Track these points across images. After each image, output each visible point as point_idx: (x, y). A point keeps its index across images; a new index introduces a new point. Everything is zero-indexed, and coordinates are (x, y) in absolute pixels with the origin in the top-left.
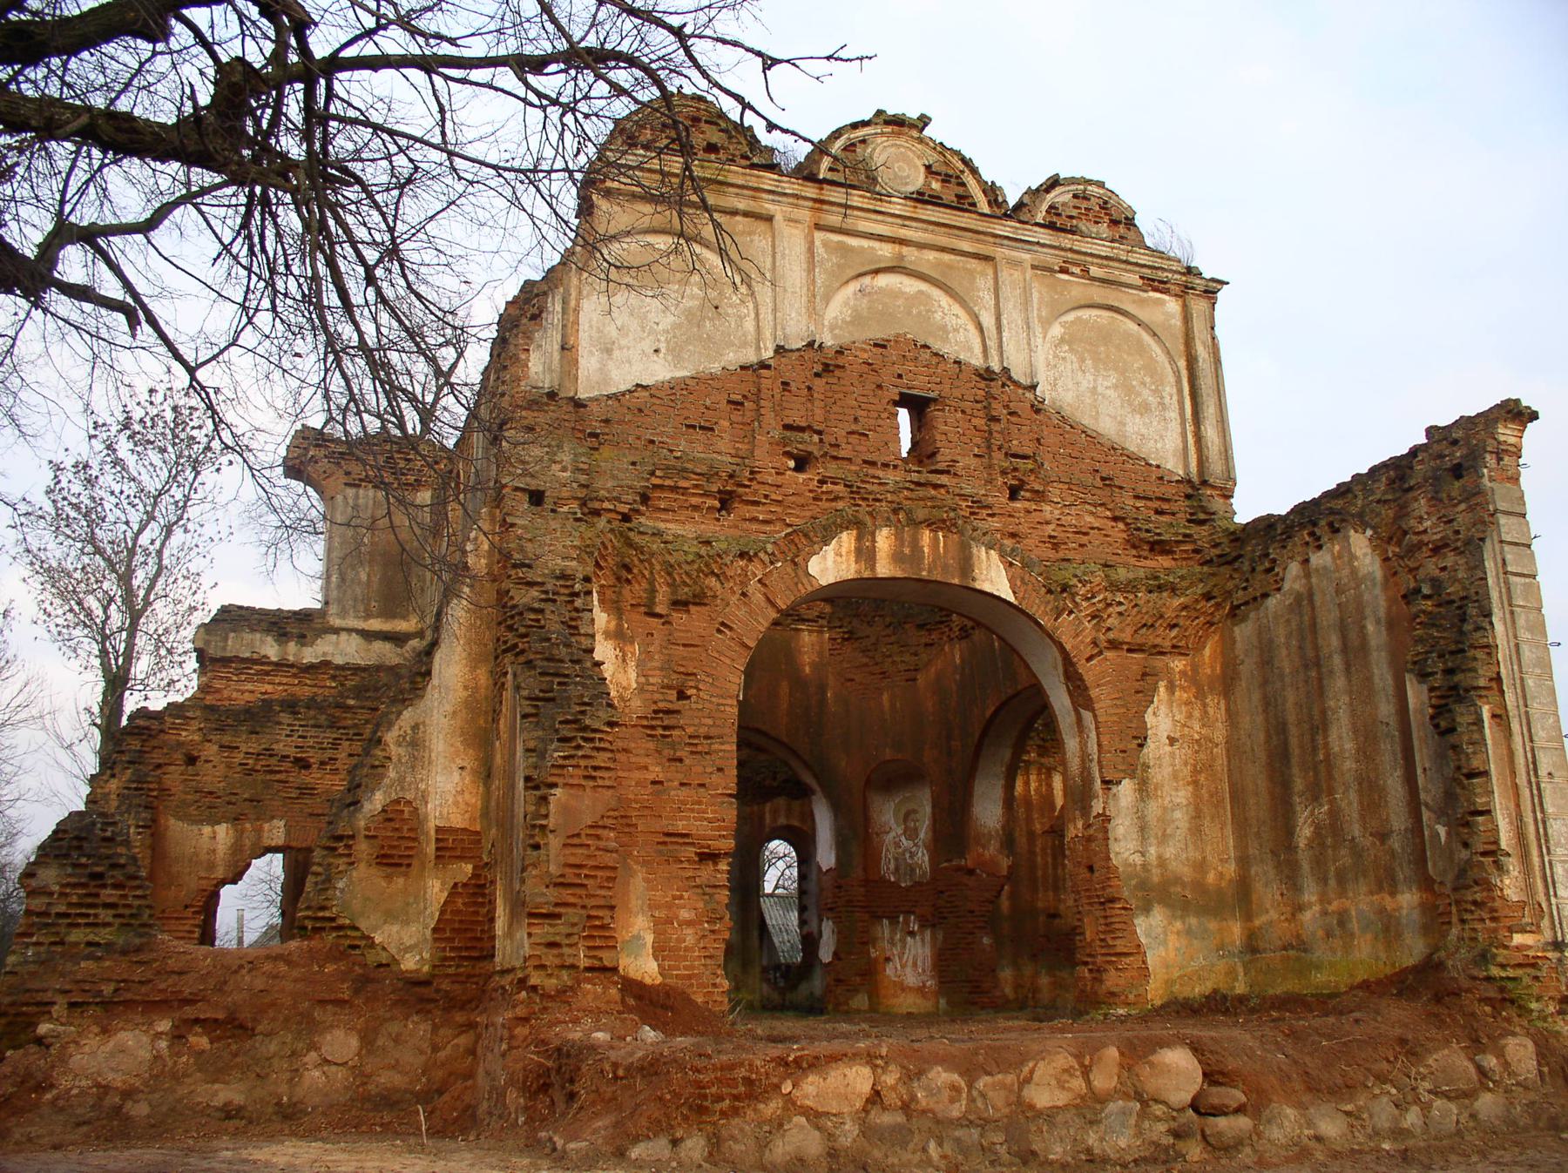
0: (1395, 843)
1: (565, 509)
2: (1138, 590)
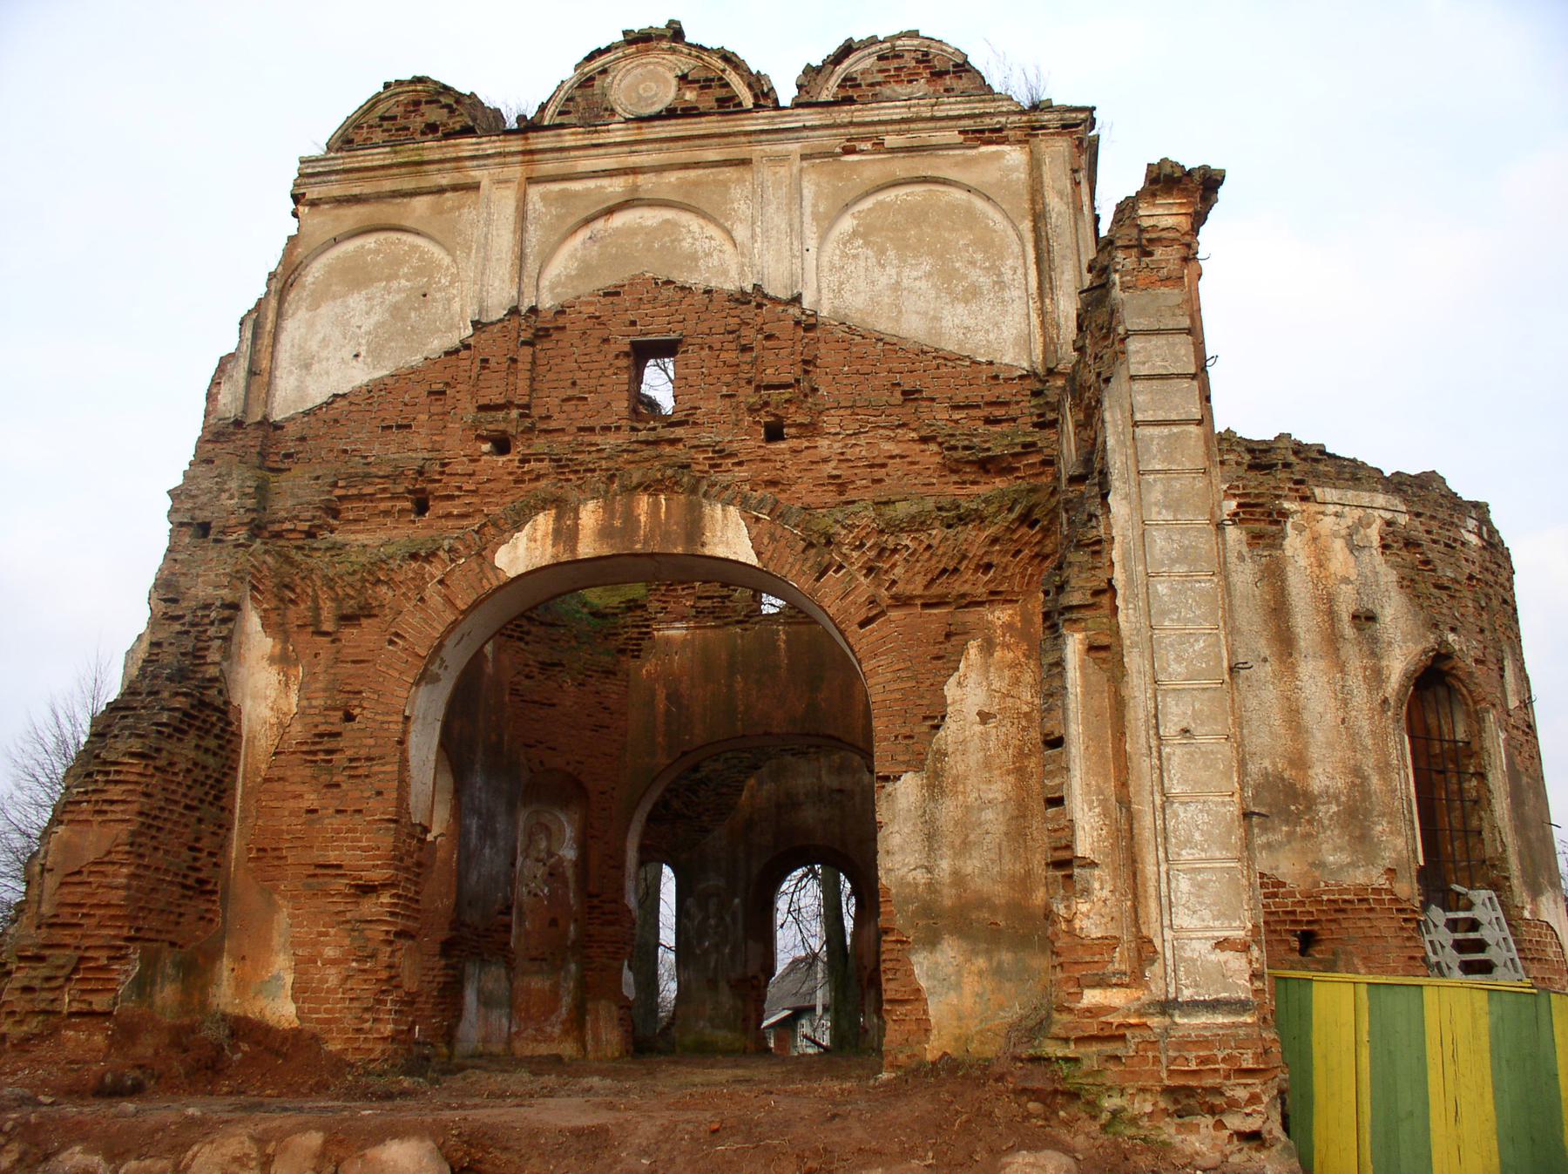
2: (931, 527)
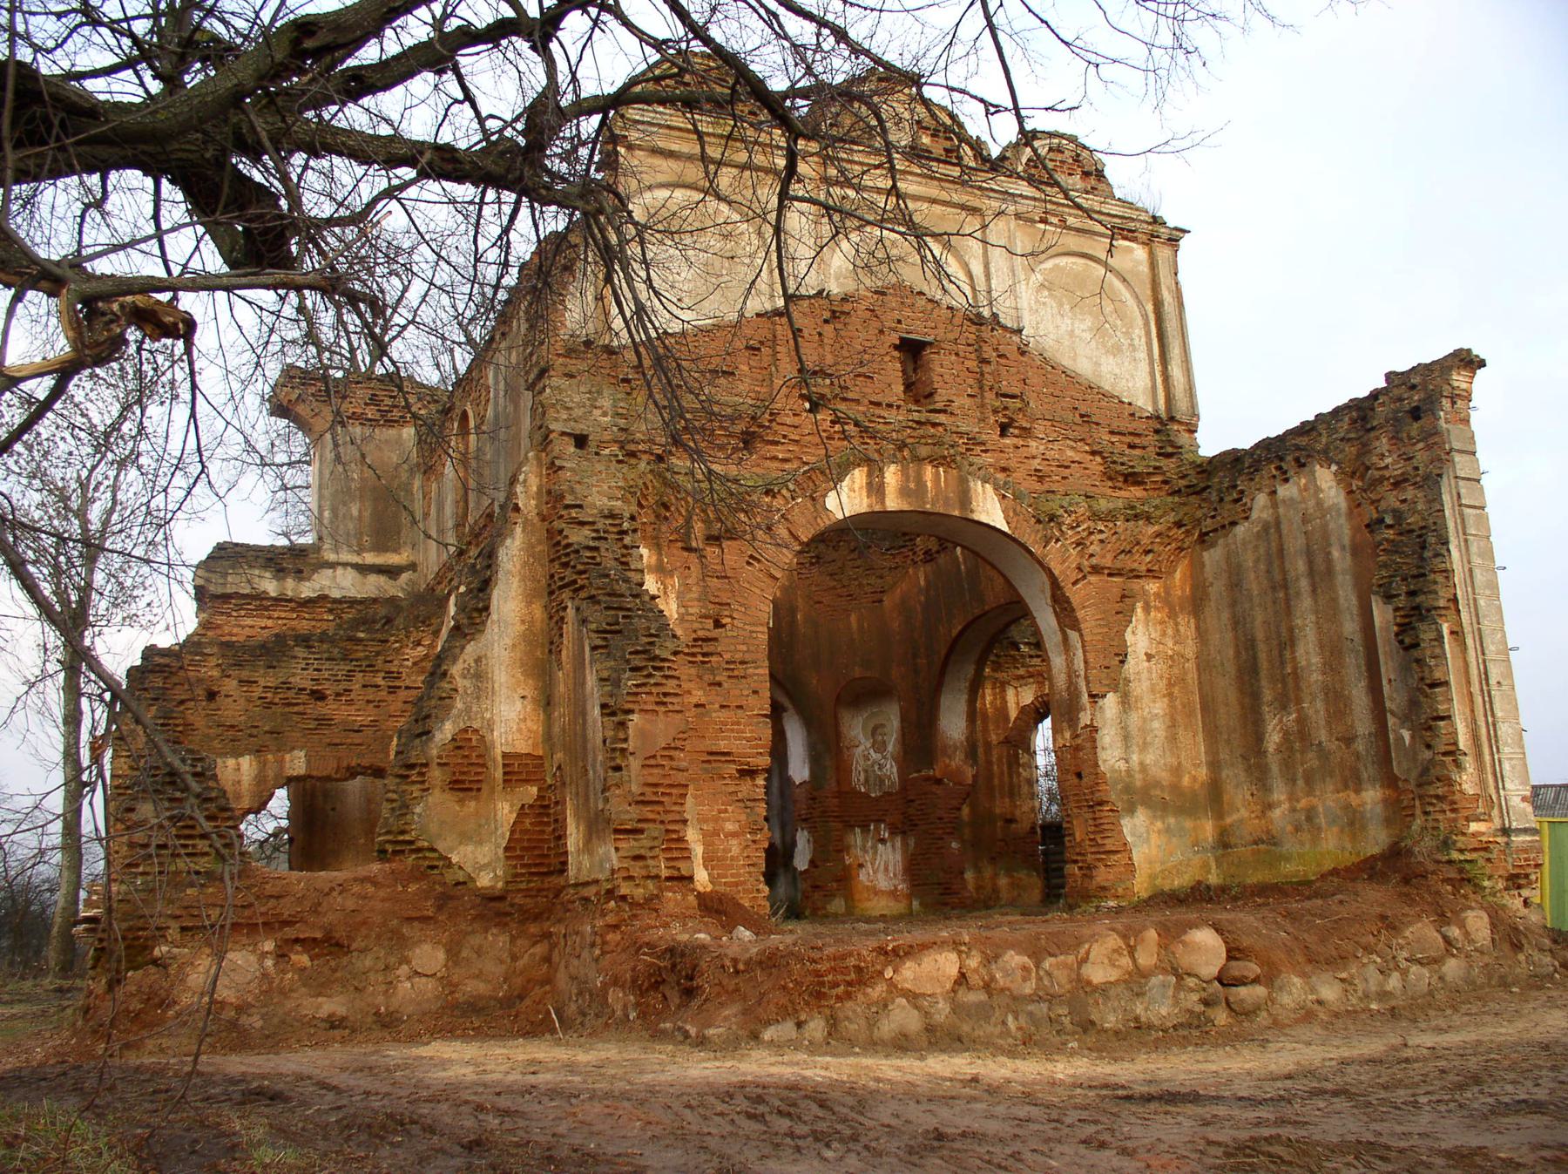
1: (607, 451)
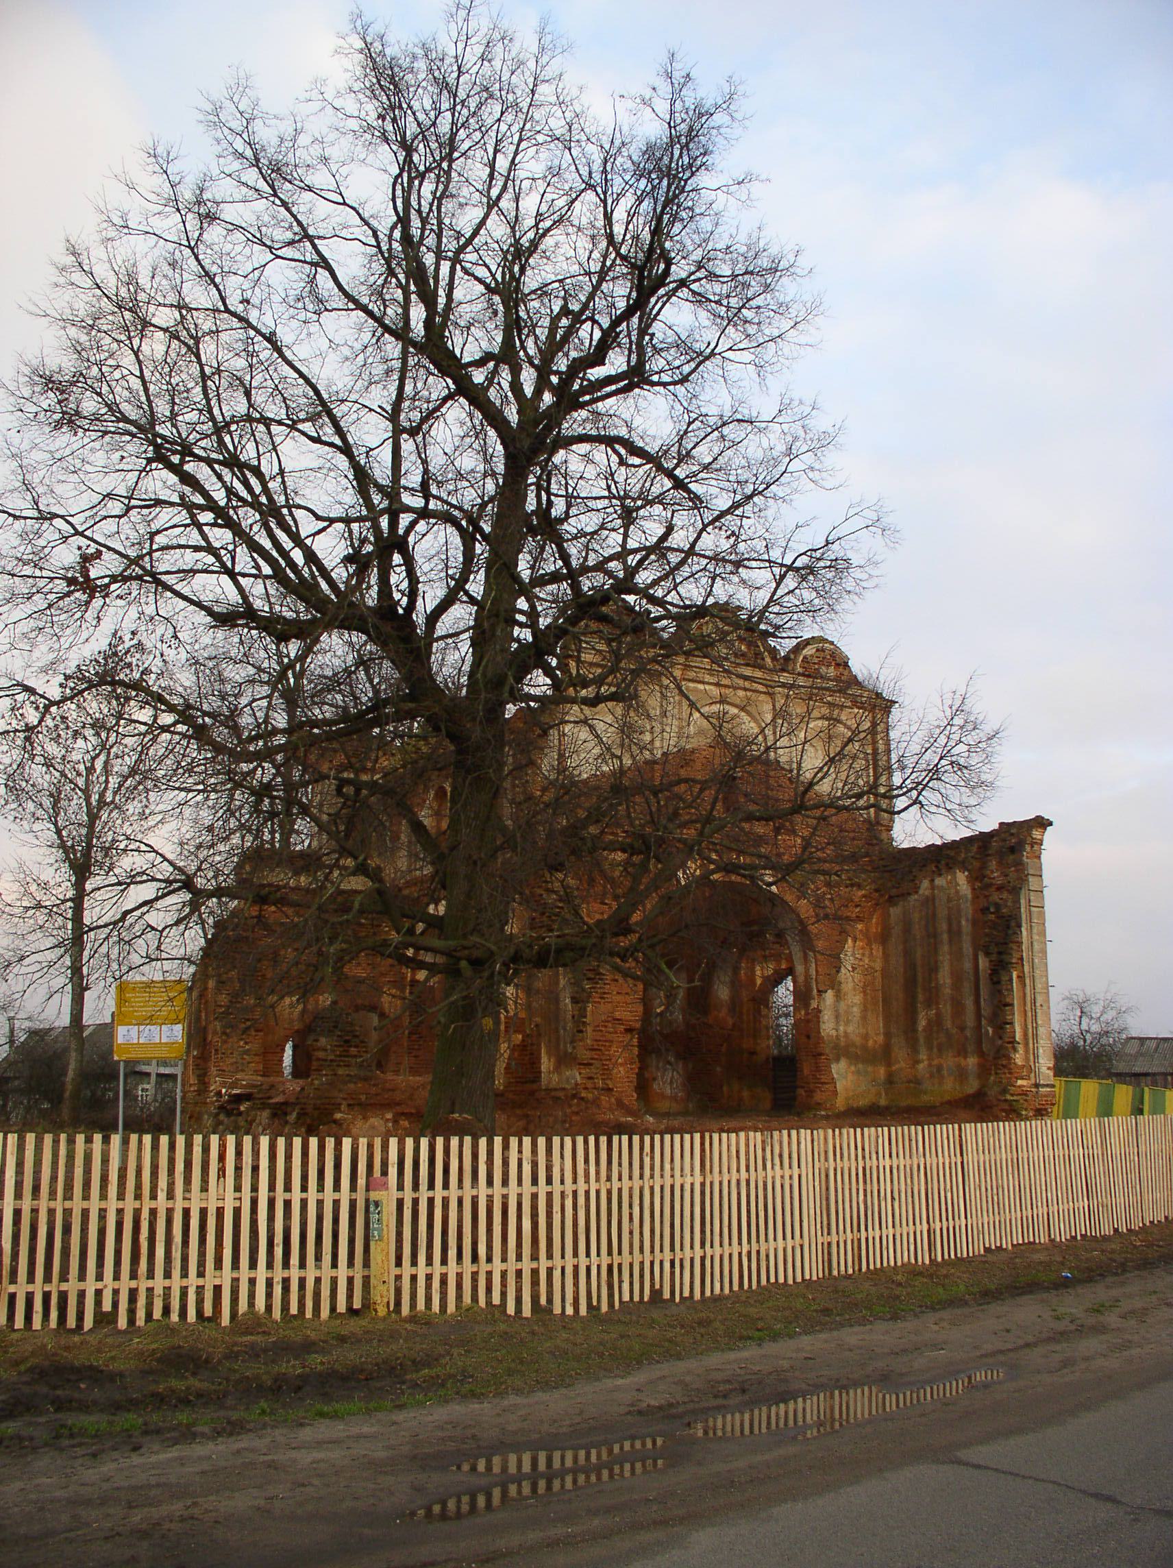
0: (968, 1033)
